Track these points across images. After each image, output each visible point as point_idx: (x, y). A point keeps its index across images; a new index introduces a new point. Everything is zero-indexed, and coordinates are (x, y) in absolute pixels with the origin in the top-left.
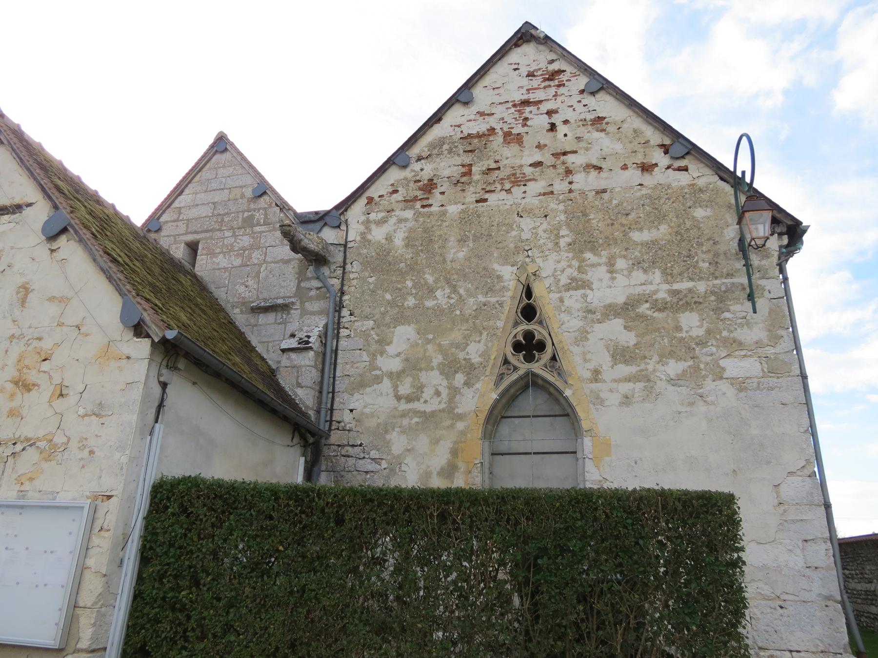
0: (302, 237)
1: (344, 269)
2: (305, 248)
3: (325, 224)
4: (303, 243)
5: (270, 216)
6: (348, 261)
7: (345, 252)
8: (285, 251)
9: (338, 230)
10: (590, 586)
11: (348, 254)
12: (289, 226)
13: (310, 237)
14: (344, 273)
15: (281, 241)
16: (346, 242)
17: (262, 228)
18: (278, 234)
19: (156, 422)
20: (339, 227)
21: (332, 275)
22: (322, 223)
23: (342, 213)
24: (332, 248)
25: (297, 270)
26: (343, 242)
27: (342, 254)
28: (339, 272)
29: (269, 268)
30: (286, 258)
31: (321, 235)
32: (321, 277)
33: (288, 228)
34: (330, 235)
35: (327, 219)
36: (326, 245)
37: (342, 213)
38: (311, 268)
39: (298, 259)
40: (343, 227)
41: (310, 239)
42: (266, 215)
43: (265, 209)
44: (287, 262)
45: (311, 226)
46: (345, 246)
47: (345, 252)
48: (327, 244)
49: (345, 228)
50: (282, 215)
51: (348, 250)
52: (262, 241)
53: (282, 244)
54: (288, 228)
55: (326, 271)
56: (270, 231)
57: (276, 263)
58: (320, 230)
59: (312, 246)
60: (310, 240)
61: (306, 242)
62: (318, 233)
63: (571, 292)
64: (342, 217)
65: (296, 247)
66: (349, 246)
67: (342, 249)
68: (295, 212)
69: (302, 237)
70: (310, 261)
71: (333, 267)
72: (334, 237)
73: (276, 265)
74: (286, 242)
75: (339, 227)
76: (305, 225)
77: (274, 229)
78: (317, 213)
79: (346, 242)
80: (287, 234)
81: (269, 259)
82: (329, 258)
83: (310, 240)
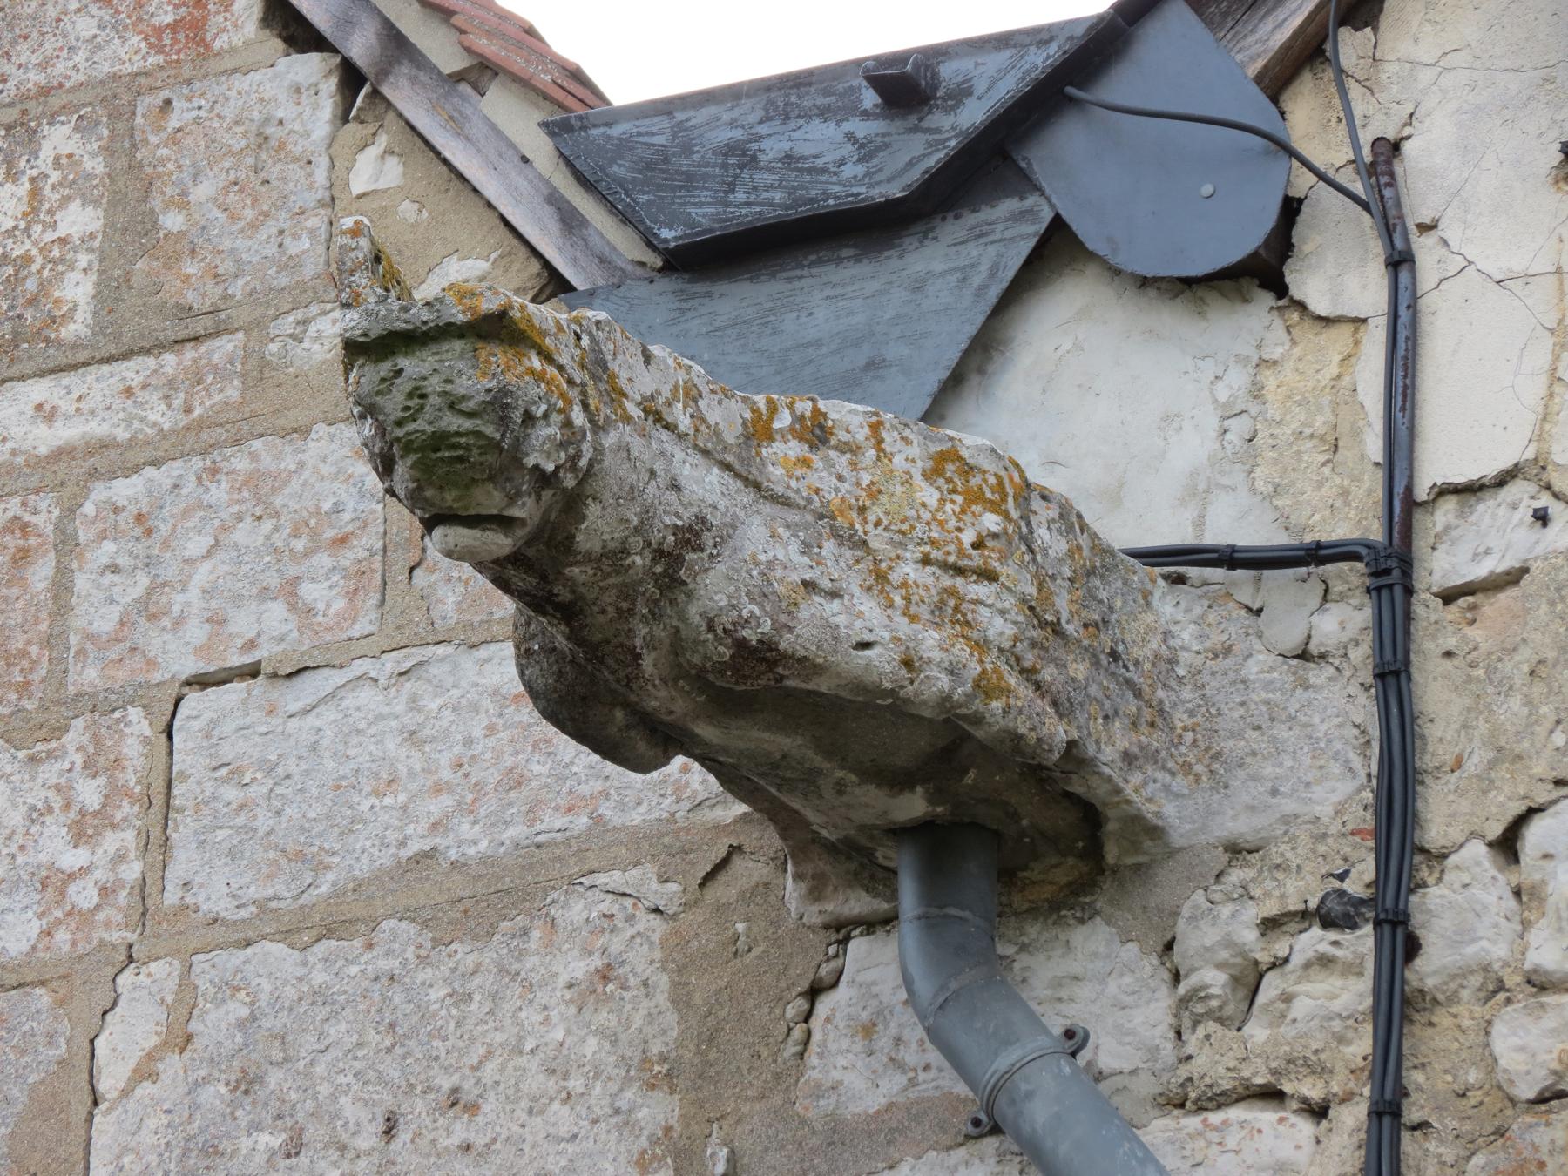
0: (706, 486)
1: (1400, 941)
2: (759, 657)
3: (1057, 249)
4: (717, 590)
5: (198, 200)
6: (1444, 814)
7: (1392, 676)
8: (447, 718)
9: (1255, 321)
10: (659, 554)
11: (1437, 693)
12: (496, 329)
13: (826, 478)
14: (1396, 1008)
15: (388, 580)
16: (1403, 506)
17: (88, 407)
18: (334, 469)
19: (306, 668)
20: (1264, 272)
21: (1214, 1059)
22: (996, 237)
23: (1310, 52)
24: (1176, 618)
25: (651, 1017)
26: (1355, 517)
27: (1343, 706)
28: (1327, 995)
29: (216, 1024)
30: (472, 840)
31: (995, 426)
32: (1044, 1103)
33: (469, 374)
34: (1129, 421)
35: (1075, 168)
36: (1089, 587)
37: (1310, 52)
38: (875, 966)
39: (661, 846)
40: (1338, 272)
41: (825, 515)
42: (131, 197)
43: (113, 106)
44: (489, 901)
45: (829, 302)
46: (1389, 569)
47: (1392, 676)
48: (1097, 562)
49: (1365, 290)
50: (374, 169)
51: (1435, 630)
52: (97, 608)
53: (414, 637)
54: (469, 374)
55: (1099, 988)
56: (198, 440)
57: (331, 924)
58: (982, 351)
59: (867, 627)
60: (833, 524)
61: (770, 571)
62: (933, 414)
63: (623, 383)
64: (1306, 115)
65: (616, 651)
66: (1452, 553)
67: (1344, 621)
68: (569, 104)
69: (706, 486)
70: (857, 858)
71: (1219, 928)
72: (1193, 446)
73: (321, 966)
74: (458, 589)
75: (1264, 272)
76: (737, 299)
77: (267, 409)
78: (903, 86)
79: (1403, 506)
80: (481, 473)
81: (208, 879)
82: (1157, 795)
83: (833, 524)
